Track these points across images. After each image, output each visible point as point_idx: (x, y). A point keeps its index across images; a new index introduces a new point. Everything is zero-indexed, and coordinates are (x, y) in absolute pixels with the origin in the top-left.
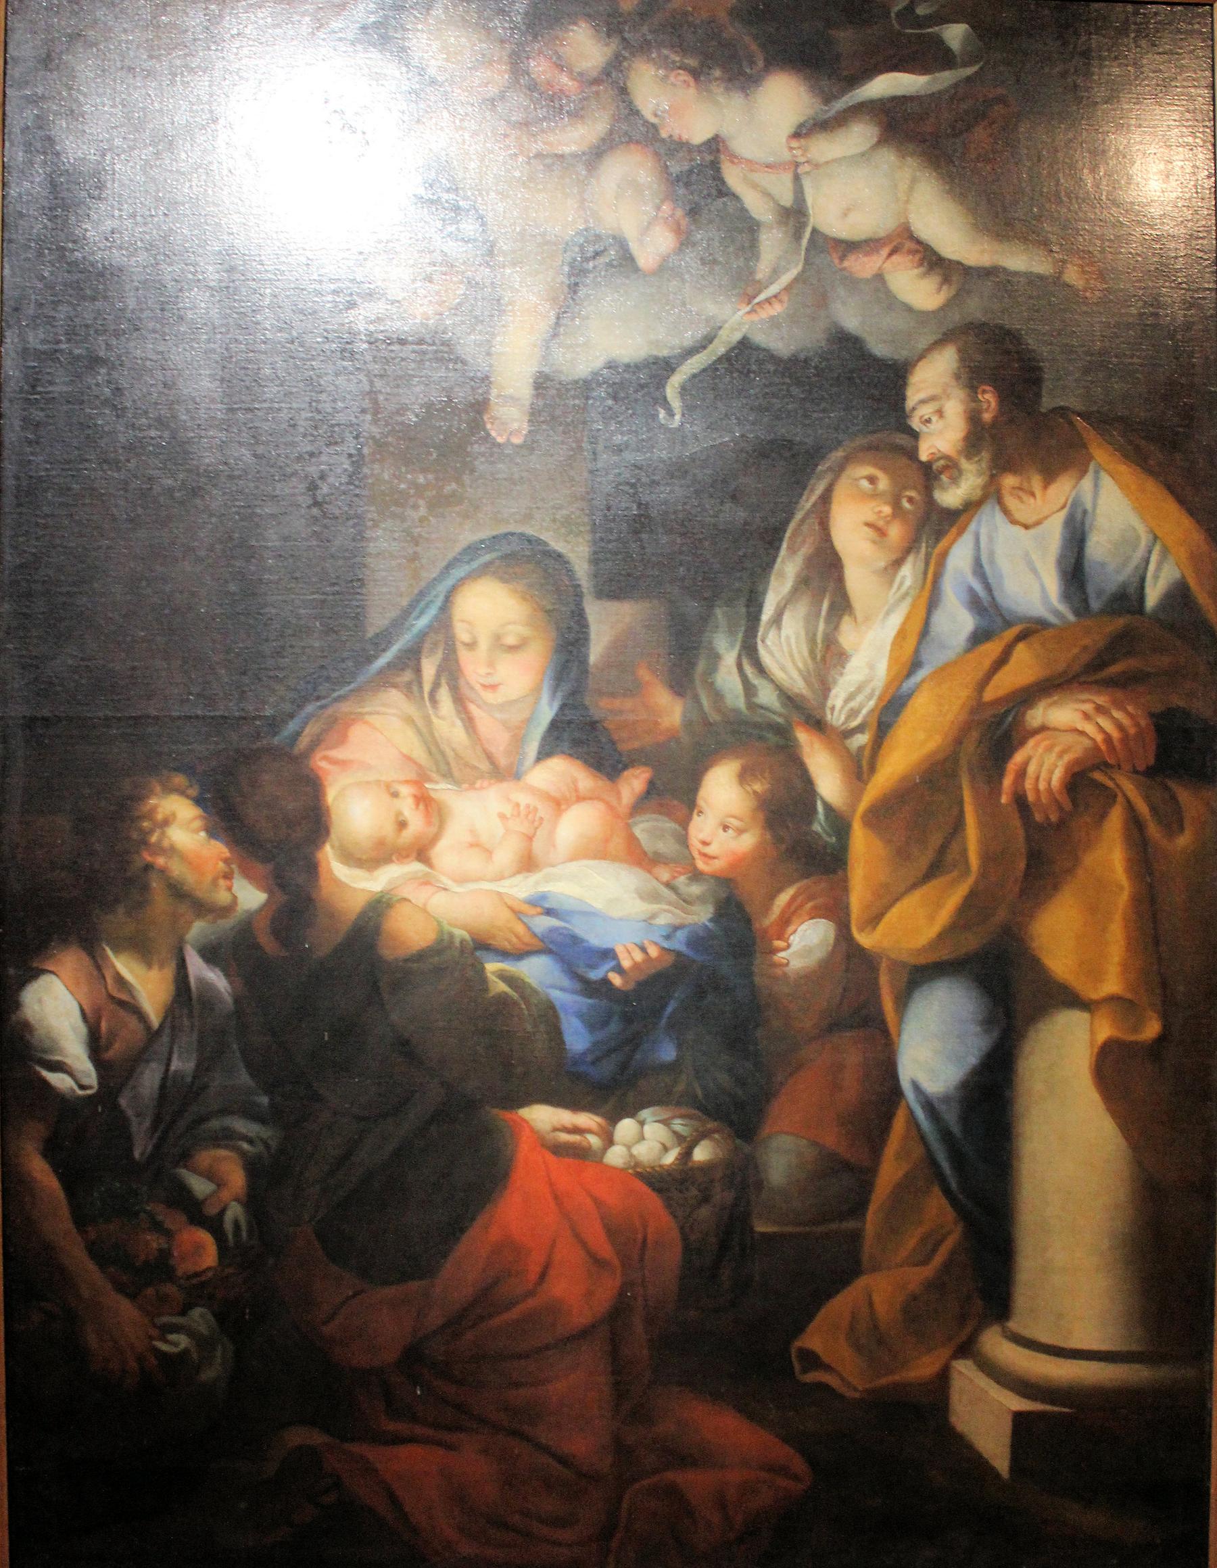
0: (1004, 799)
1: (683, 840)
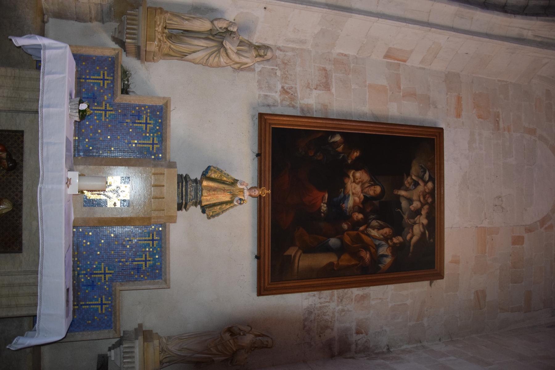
0: (360, 249)
1: (356, 212)
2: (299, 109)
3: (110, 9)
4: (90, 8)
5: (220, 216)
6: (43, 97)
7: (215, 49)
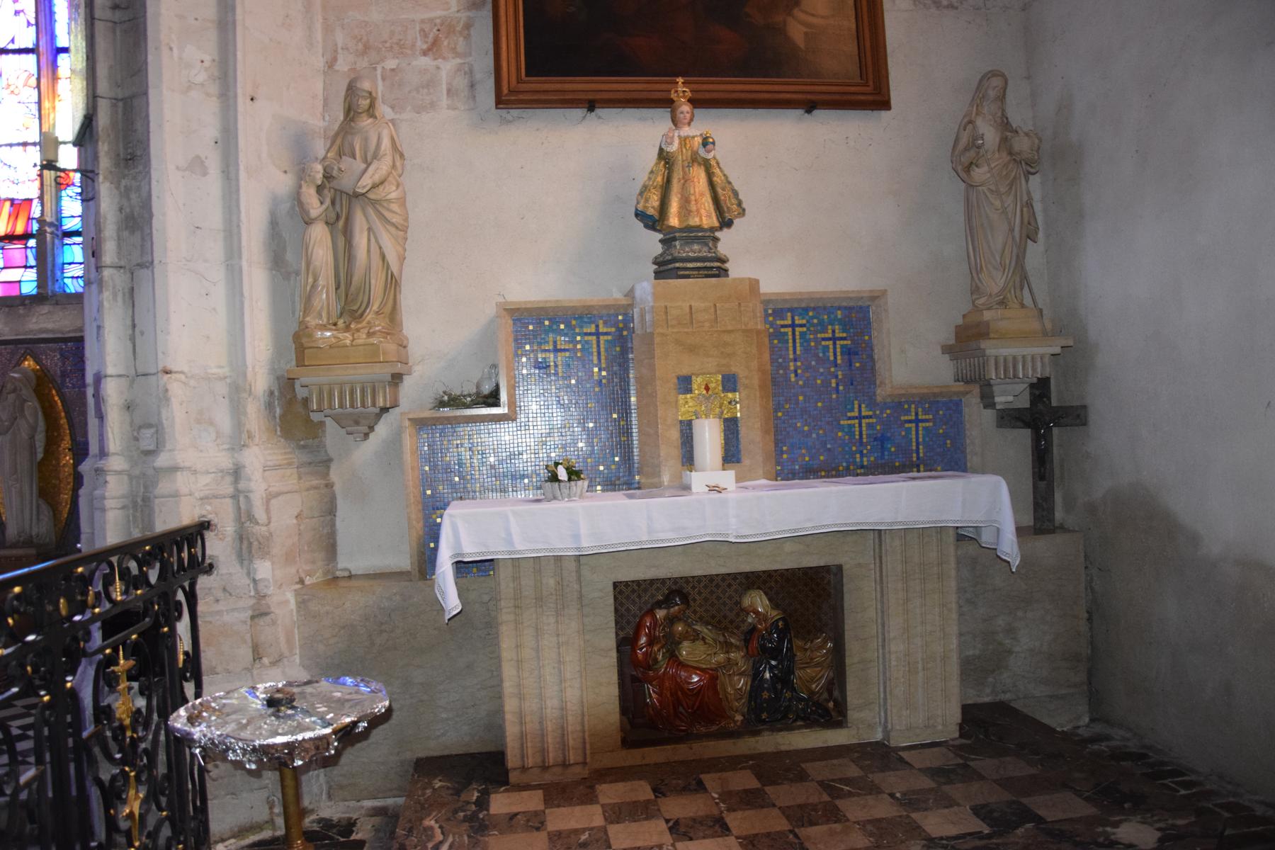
2: (470, 14)
3: (304, 447)
4: (308, 490)
5: (736, 188)
6: (560, 549)
7: (370, 211)
